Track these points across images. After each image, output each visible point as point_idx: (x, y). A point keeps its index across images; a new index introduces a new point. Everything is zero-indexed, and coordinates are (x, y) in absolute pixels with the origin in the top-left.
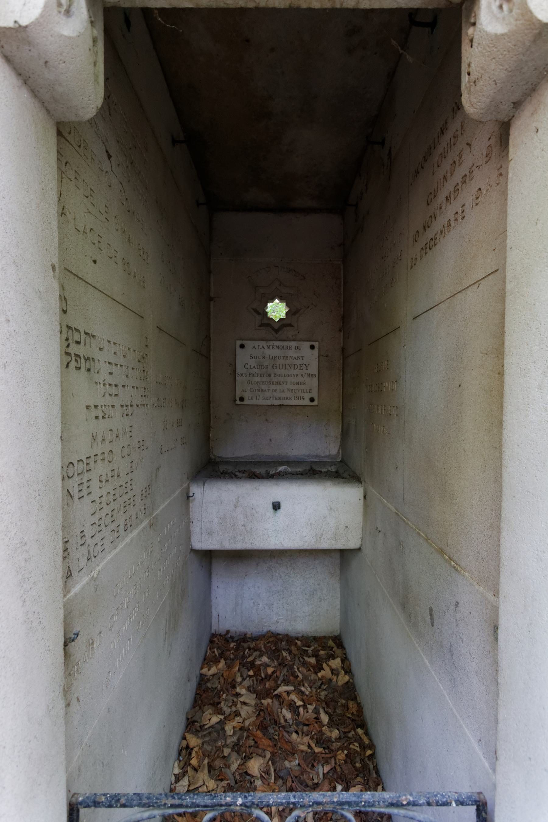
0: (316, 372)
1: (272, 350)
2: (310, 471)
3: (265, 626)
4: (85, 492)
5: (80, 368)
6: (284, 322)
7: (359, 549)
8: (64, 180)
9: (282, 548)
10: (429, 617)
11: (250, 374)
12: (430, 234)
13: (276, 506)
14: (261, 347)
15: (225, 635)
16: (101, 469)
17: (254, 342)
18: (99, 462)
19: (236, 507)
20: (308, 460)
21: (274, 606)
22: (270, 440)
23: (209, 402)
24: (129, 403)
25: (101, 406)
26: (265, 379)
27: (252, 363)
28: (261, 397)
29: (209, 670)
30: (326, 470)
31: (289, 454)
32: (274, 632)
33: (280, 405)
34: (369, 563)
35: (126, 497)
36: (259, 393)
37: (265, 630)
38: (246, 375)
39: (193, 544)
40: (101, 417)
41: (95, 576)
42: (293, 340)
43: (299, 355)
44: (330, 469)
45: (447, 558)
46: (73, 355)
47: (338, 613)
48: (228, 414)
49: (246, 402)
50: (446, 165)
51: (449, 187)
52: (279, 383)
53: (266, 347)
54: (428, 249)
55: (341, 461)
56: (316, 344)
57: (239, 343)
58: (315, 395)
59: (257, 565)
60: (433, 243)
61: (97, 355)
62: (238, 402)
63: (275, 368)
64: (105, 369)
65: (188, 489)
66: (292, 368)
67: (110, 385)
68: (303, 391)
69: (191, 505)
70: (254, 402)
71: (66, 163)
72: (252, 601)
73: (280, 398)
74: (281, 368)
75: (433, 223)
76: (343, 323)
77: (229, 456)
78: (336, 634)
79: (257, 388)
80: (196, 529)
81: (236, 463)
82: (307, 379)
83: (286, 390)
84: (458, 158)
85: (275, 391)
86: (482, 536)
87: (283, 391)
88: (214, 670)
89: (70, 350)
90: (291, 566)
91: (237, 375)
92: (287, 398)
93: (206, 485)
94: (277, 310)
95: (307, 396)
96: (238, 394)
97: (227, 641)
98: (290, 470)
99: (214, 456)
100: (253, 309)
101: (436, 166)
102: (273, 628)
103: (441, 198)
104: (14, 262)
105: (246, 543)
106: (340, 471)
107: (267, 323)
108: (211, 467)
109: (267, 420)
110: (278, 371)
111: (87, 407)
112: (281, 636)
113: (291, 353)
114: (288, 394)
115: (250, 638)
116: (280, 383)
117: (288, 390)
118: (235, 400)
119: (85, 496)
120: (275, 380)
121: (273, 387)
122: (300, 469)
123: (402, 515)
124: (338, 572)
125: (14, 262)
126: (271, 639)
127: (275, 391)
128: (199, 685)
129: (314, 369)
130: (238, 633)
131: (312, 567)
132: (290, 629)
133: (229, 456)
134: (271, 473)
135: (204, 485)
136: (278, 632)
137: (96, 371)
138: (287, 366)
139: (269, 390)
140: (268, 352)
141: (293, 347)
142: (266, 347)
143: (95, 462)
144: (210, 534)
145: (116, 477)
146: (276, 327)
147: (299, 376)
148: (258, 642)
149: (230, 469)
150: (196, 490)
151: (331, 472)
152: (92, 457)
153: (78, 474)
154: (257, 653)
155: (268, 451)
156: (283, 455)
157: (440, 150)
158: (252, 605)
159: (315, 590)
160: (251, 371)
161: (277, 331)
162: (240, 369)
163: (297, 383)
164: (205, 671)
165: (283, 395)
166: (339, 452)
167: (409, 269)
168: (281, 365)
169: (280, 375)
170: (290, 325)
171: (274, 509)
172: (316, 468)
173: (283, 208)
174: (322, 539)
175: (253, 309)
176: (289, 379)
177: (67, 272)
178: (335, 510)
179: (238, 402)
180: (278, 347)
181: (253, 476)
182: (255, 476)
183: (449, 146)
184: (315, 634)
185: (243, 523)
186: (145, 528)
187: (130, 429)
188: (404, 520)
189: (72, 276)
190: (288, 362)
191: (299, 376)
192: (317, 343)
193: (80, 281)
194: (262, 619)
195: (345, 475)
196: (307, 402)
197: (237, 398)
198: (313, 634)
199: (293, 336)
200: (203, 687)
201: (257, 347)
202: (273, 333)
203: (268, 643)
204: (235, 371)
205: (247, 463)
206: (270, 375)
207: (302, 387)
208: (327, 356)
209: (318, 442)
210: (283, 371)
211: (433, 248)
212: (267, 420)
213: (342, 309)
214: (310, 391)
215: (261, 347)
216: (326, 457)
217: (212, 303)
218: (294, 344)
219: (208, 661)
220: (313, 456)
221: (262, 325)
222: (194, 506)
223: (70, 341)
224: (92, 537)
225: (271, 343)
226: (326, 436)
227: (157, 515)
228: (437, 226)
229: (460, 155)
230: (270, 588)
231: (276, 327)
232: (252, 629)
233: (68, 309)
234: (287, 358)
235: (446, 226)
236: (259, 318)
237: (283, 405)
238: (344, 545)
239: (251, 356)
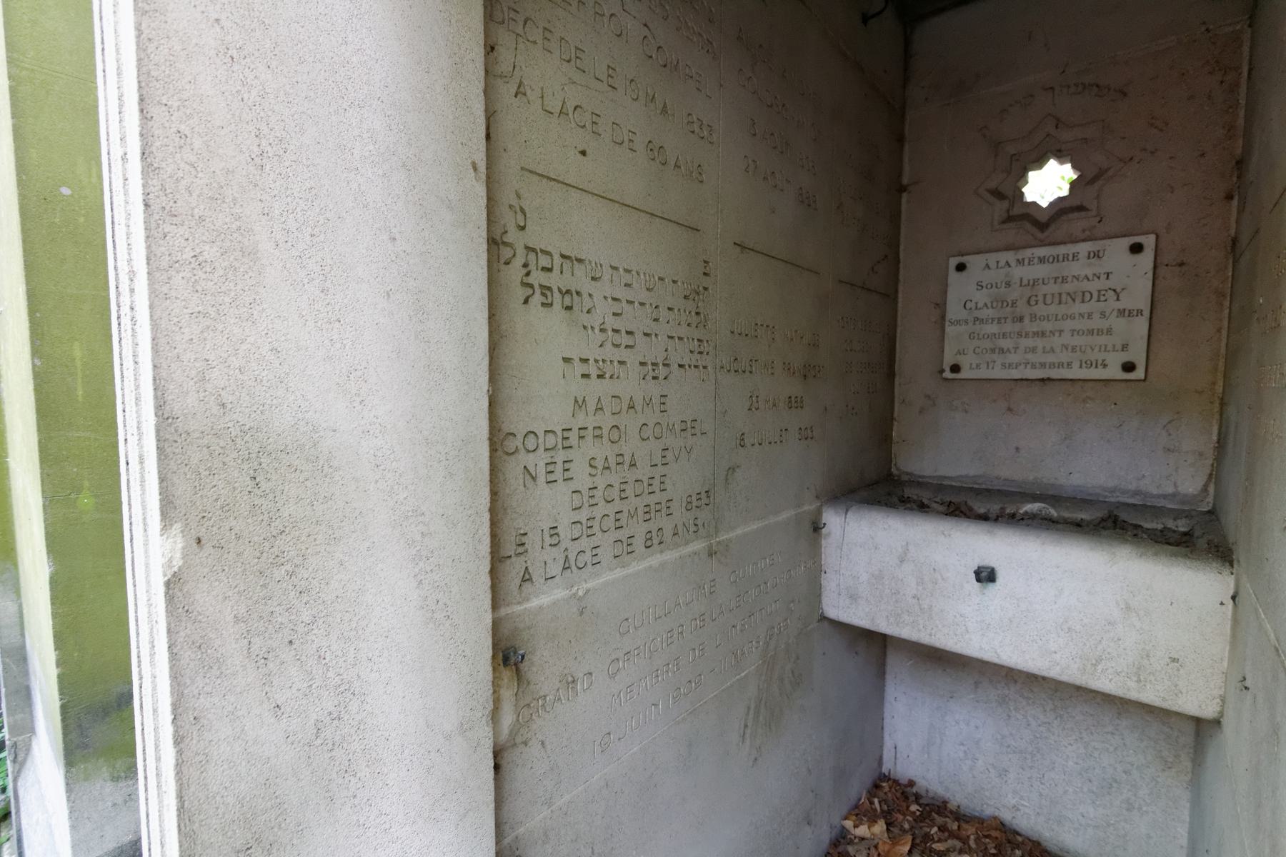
1: (1030, 266)
4: (559, 474)
5: (551, 305)
6: (1067, 204)
8: (521, 46)
9: (996, 660)
11: (976, 319)
14: (1002, 263)
15: (906, 786)
16: (591, 448)
18: (590, 438)
19: (902, 561)
20: (1112, 500)
23: (891, 374)
24: (660, 361)
25: (596, 361)
27: (981, 297)
29: (855, 826)
30: (1160, 527)
32: (1007, 823)
33: (1042, 380)
37: (989, 812)
38: (966, 322)
40: (594, 376)
41: (581, 593)
42: (1084, 240)
43: (1097, 270)
46: (536, 286)
48: (928, 397)
49: (963, 374)
53: (1013, 264)
55: (1209, 512)
56: (1149, 241)
57: (954, 262)
58: (1137, 354)
59: (977, 684)
61: (586, 286)
63: (1033, 303)
64: (603, 310)
65: (819, 512)
66: (1078, 300)
70: (983, 373)
71: (525, 23)
73: (1043, 365)
74: (1049, 302)
77: (927, 474)
80: (830, 584)
81: (940, 487)
82: (1119, 324)
85: (1033, 350)
87: (1052, 350)
88: (863, 830)
89: (530, 280)
92: (1061, 365)
95: (1115, 362)
96: (948, 360)
97: (905, 796)
99: (898, 469)
100: (988, 191)
102: (1006, 816)
104: (404, 166)
106: (1196, 533)
109: (1010, 409)
111: (567, 360)
112: (1020, 839)
113: (1075, 268)
114: (1064, 357)
115: (951, 812)
117: (1065, 347)
118: (942, 371)
119: (560, 481)
121: (1029, 342)
125: (404, 166)
126: (994, 833)
127: (1033, 350)
128: (835, 843)
129: (1139, 296)
130: (931, 794)
131: (1110, 729)
132: (1047, 834)
136: (1015, 827)
137: (585, 310)
138: (1064, 296)
139: (1016, 348)
140: (1018, 272)
142: (1013, 264)
143: (581, 437)
144: (854, 598)
145: (626, 466)
148: (964, 826)
149: (925, 496)
150: (833, 520)
151: (1174, 531)
152: (575, 430)
153: (546, 450)
154: (958, 844)
156: (1045, 480)
158: (961, 755)
162: (954, 310)
163: (1091, 332)
164: (849, 824)
165: (1050, 358)
166: (1205, 489)
168: (1049, 297)
170: (1081, 208)
172: (1123, 516)
174: (1100, 668)
175: (988, 191)
176: (1068, 325)
177: (526, 173)
178: (1142, 613)
179: (948, 374)
180: (1042, 260)
185: (914, 592)
189: (536, 178)
190: (1068, 287)
192: (1152, 238)
193: (553, 183)
196: (1115, 372)
199: (1084, 231)
200: (841, 849)
201: (993, 265)
203: (986, 837)
204: (943, 317)
206: (1021, 319)
207: (1102, 340)
208: (1182, 264)
209: (1164, 468)
210: (1053, 309)
212: (1010, 409)
213: (1240, 142)
214: (1124, 347)
215: (1002, 263)
217: (905, 195)
218: (1084, 248)
219: (860, 812)
220: (1124, 492)
221: (1009, 219)
223: (532, 267)
225: (1028, 253)
226: (1168, 450)
227: (730, 540)
230: (1003, 737)
232: (959, 797)
233: (529, 223)
234: (1064, 280)
236: (1000, 207)
237: (1049, 379)
238: (1164, 699)
239: (980, 286)
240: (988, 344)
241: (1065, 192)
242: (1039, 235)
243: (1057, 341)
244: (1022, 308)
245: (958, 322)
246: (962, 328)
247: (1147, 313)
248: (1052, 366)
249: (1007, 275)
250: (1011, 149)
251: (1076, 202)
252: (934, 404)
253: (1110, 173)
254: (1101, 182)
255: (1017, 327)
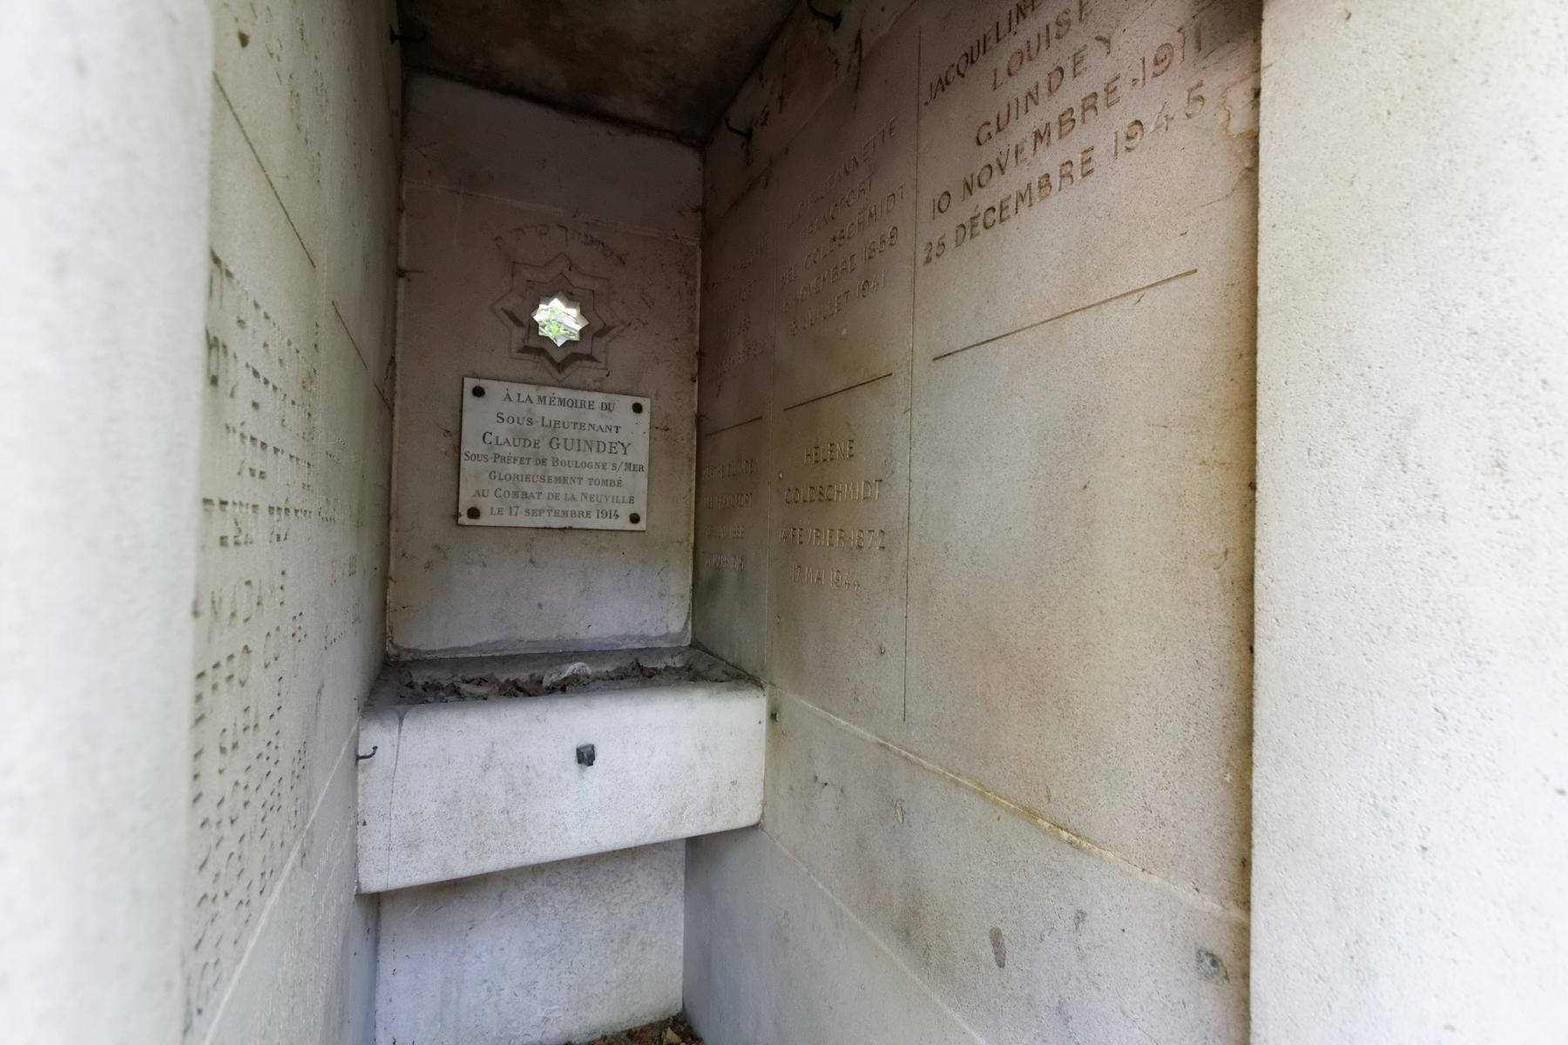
0: (644, 462)
1: (549, 406)
2: (636, 671)
3: (515, 1038)
6: (578, 349)
7: (755, 827)
10: (990, 948)
11: (497, 456)
12: (984, 199)
13: (586, 757)
14: (523, 398)
17: (507, 385)
18: (223, 686)
19: (486, 768)
21: (540, 985)
22: (540, 605)
26: (531, 469)
27: (502, 431)
28: (522, 509)
31: (582, 635)
34: (787, 852)
35: (268, 786)
36: (518, 501)
39: (363, 880)
40: (231, 541)
44: (670, 663)
45: (1046, 825)
47: (678, 967)
48: (436, 547)
50: (1035, 74)
51: (1046, 112)
52: (563, 480)
53: (535, 400)
54: (980, 227)
56: (646, 403)
57: (470, 384)
60: (992, 216)
62: (464, 519)
67: (253, 439)
68: (616, 500)
69: (360, 776)
70: (505, 520)
72: (485, 986)
73: (565, 513)
75: (994, 179)
76: (700, 366)
78: (674, 1012)
79: (512, 489)
80: (373, 839)
81: (456, 662)
82: (625, 475)
83: (578, 497)
84: (1070, 63)
85: (556, 496)
86: (1159, 775)
87: (573, 498)
90: (580, 885)
91: (463, 457)
93: (406, 722)
94: (559, 319)
95: (625, 511)
98: (589, 670)
99: (396, 647)
100: (506, 312)
101: (1002, 73)
103: (1022, 130)
105: (509, 853)
106: (702, 663)
107: (536, 346)
108: (404, 680)
110: (561, 454)
113: (593, 417)
114: (583, 506)
116: (565, 480)
117: (584, 495)
118: (457, 515)
120: (554, 472)
121: (548, 488)
122: (608, 668)
123: (900, 746)
124: (681, 877)
127: (556, 496)
129: (640, 452)
133: (438, 646)
134: (547, 682)
135: (401, 720)
140: (541, 411)
141: (597, 405)
142: (535, 400)
146: (558, 357)
147: (609, 467)
149: (442, 677)
150: (378, 736)
155: (534, 630)
157: (1016, 43)
158: (483, 995)
159: (632, 928)
160: (497, 450)
161: (560, 367)
162: (470, 443)
163: (605, 482)
165: (571, 506)
167: (920, 262)
169: (568, 464)
170: (590, 358)
171: (580, 761)
172: (648, 664)
173: (578, 106)
176: (587, 473)
179: (464, 519)
180: (562, 402)
181: (517, 691)
182: (519, 689)
183: (1043, 39)
184: (631, 1025)
186: (293, 869)
187: (278, 581)
188: (906, 758)
190: (585, 435)
191: (609, 467)
194: (510, 1022)
195: (716, 672)
197: (463, 511)
198: (625, 1027)
202: (552, 368)
205: (481, 661)
206: (543, 462)
207: (614, 491)
209: (654, 611)
210: (573, 455)
211: (997, 225)
212: (532, 562)
214: (631, 500)
215: (523, 398)
216: (660, 638)
218: (598, 398)
221: (526, 350)
222: (373, 777)
224: (197, 946)
226: (662, 595)
228: (1001, 188)
229: (1077, 59)
231: (558, 357)
234: (582, 425)
235: (1035, 186)
236: (519, 333)
240: (509, 486)
241: (574, 312)
242: (557, 375)
243: (578, 489)
244: (544, 451)
245: (477, 457)
246: (481, 465)
247: (646, 468)
248: (573, 514)
249: (529, 411)
250: (527, 274)
251: (584, 349)
252: (445, 557)
253: (614, 332)
254: (606, 338)
255: (539, 470)
